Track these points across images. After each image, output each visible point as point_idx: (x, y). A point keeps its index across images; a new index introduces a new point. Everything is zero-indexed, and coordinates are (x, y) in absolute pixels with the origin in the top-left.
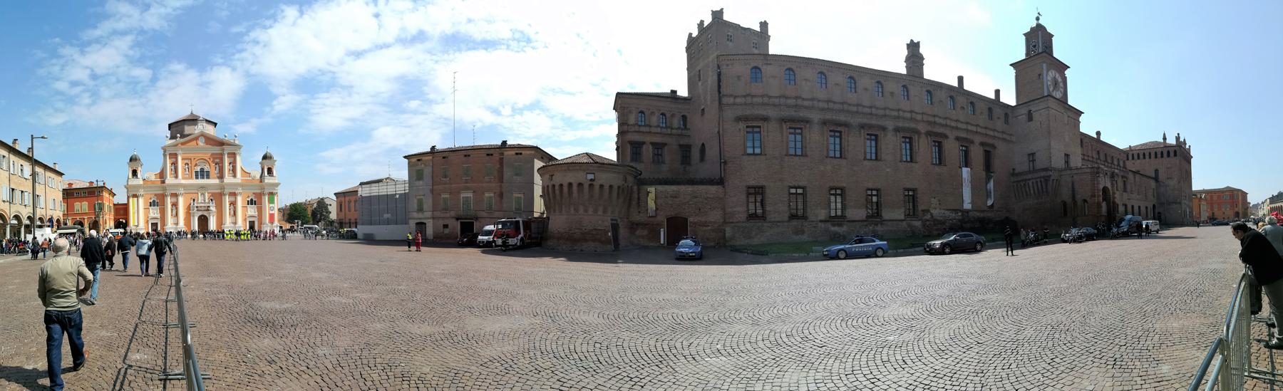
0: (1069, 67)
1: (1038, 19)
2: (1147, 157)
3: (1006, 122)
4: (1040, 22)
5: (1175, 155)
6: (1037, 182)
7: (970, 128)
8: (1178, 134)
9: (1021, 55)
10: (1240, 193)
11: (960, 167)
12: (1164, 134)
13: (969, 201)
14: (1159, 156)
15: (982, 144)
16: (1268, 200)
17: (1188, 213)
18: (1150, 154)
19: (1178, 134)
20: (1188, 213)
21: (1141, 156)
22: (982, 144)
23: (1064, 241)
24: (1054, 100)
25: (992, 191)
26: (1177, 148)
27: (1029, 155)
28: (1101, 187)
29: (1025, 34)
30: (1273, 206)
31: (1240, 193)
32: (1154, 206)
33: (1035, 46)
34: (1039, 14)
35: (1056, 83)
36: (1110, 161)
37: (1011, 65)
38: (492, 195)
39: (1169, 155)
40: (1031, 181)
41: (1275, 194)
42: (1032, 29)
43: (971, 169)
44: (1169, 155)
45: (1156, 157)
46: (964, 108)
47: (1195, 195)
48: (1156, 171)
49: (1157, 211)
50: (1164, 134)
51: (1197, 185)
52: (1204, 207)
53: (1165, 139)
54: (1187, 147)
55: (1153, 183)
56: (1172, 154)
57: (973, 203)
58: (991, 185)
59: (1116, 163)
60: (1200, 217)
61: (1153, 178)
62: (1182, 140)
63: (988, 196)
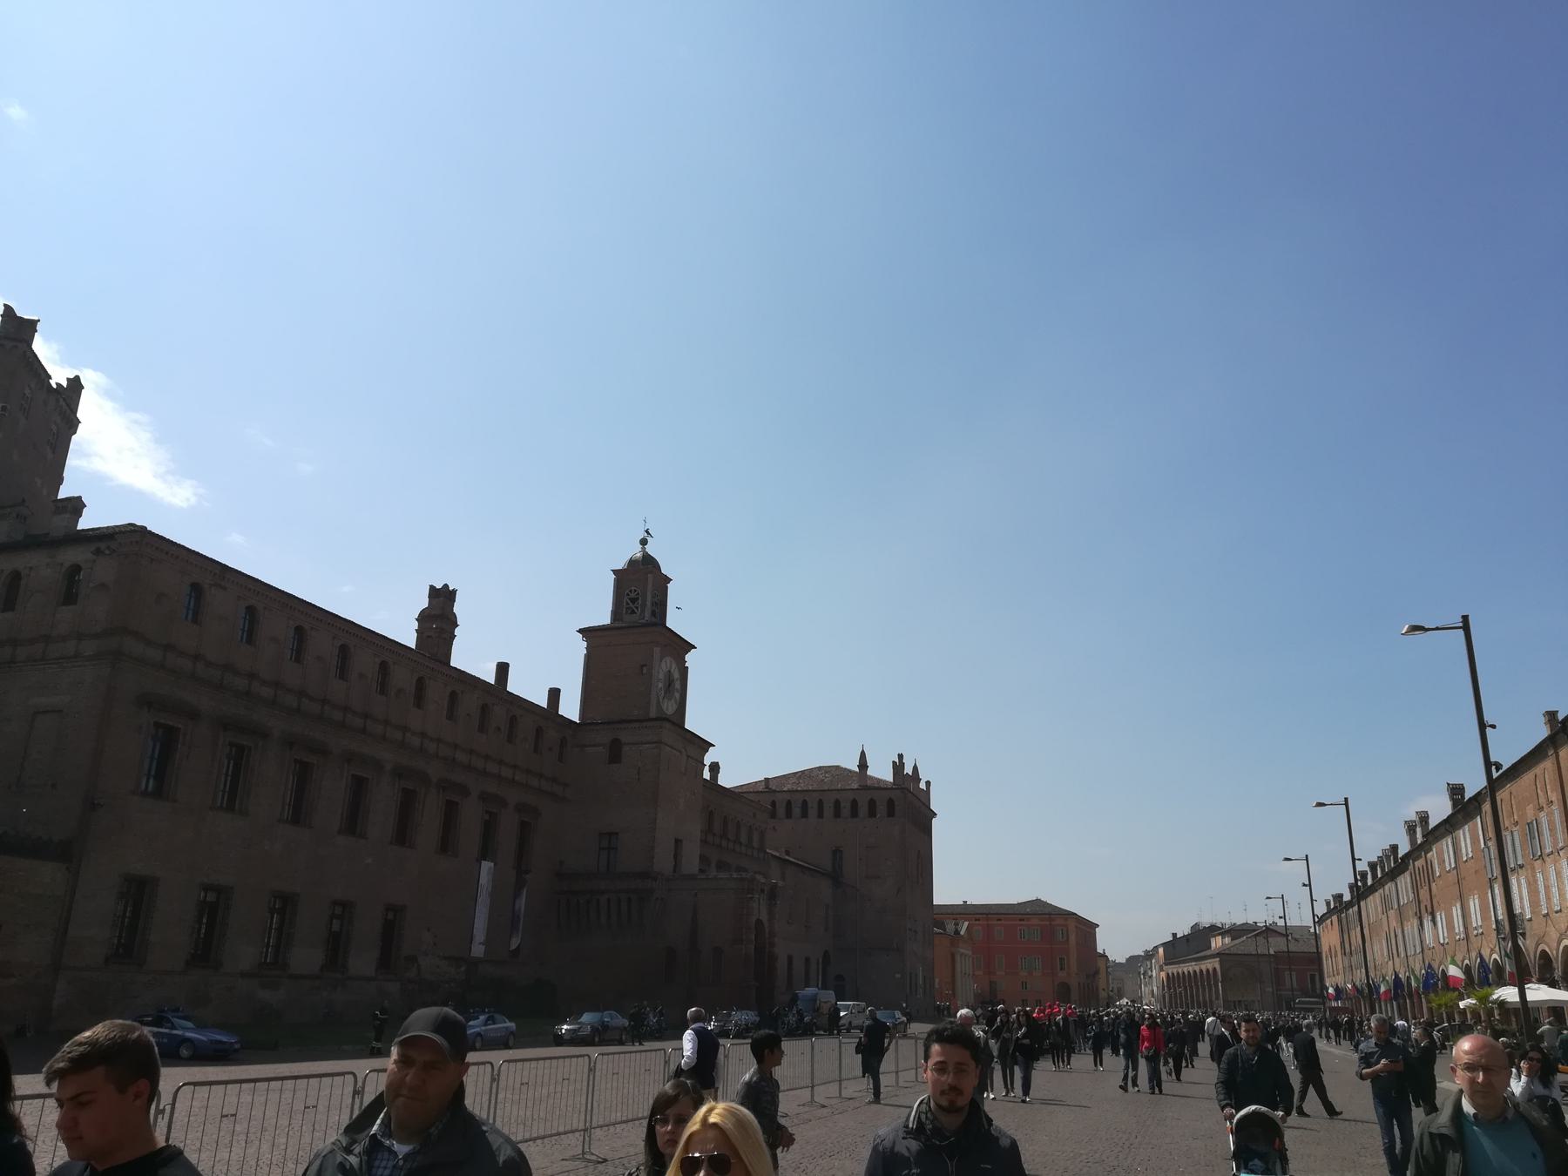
1: (644, 542)
2: (813, 812)
4: (650, 549)
5: (891, 812)
8: (901, 756)
9: (601, 614)
12: (863, 754)
16: (1161, 950)
17: (921, 981)
20: (921, 981)
21: (797, 811)
23: (559, 1041)
28: (754, 919)
30: (1173, 969)
32: (826, 955)
33: (634, 601)
34: (647, 532)
37: (580, 631)
39: (872, 812)
41: (1183, 930)
42: (632, 562)
44: (872, 812)
45: (837, 814)
46: (499, 729)
47: (941, 925)
48: (837, 853)
50: (863, 754)
51: (946, 891)
54: (922, 786)
56: (882, 809)
58: (522, 903)
59: (744, 839)
62: (908, 770)
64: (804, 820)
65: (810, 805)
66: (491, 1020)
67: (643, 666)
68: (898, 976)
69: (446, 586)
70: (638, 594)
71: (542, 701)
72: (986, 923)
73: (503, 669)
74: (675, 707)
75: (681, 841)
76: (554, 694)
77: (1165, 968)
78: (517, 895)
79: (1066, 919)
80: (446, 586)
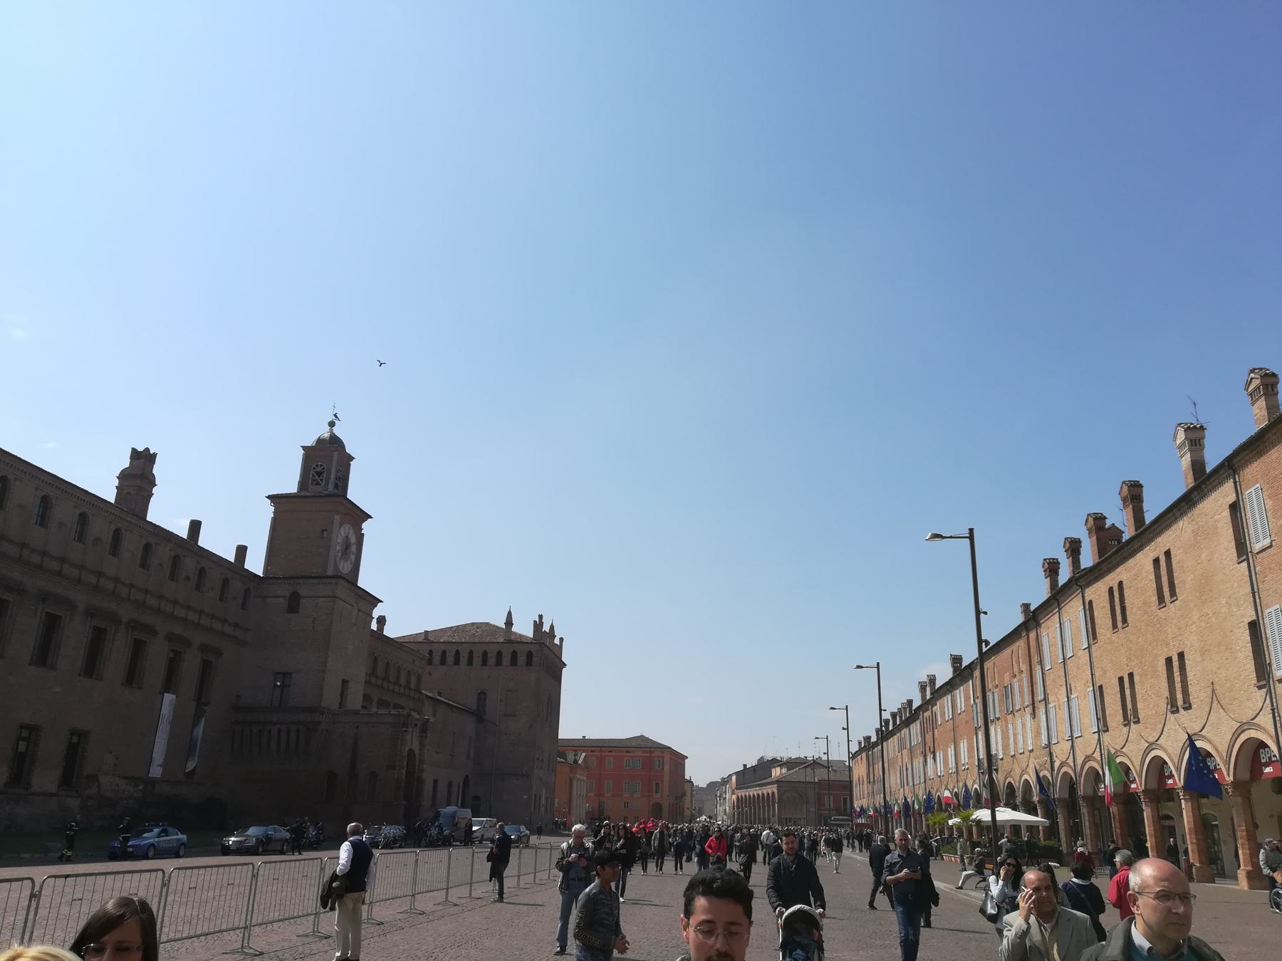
0: (370, 517)
1: (332, 424)
2: (464, 661)
4: (336, 430)
5: (529, 662)
6: (289, 731)
8: (541, 617)
10: (667, 756)
12: (510, 614)
13: (161, 761)
14: (492, 661)
16: (734, 778)
17: (543, 801)
18: (471, 653)
19: (541, 617)
20: (543, 801)
26: (533, 648)
28: (407, 749)
30: (742, 793)
31: (667, 756)
32: (466, 778)
33: (319, 474)
34: (335, 415)
35: (347, 547)
36: (392, 679)
37: (269, 497)
38: (768, 831)
39: (499, 662)
47: (563, 755)
48: (482, 695)
50: (510, 614)
51: (572, 725)
52: (581, 786)
53: (509, 623)
54: (557, 641)
55: (470, 725)
56: (522, 659)
57: (164, 765)
59: (403, 681)
60: (570, 813)
62: (546, 628)
63: (190, 752)
64: (456, 667)
65: (462, 655)
67: (323, 531)
68: (525, 797)
69: (147, 450)
70: (324, 468)
71: (231, 557)
72: (599, 754)
73: (195, 526)
74: (350, 567)
75: (348, 681)
76: (242, 551)
77: (736, 791)
78: (195, 723)
80: (147, 450)
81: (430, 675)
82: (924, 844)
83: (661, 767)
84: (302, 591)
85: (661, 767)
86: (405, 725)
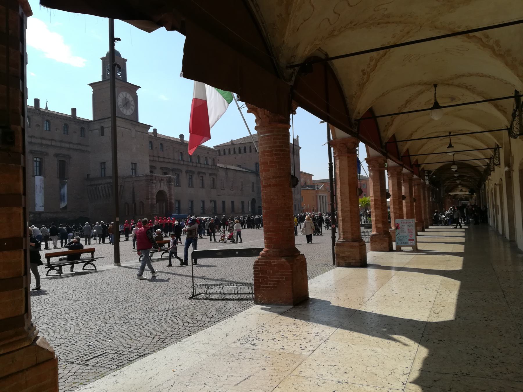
0: (140, 87)
2: (248, 151)
3: (83, 135)
7: (44, 142)
11: (34, 176)
15: (56, 155)
21: (242, 151)
22: (56, 155)
24: (122, 120)
25: (66, 195)
27: (101, 163)
29: (102, 59)
35: (126, 103)
37: (89, 85)
40: (101, 186)
43: (45, 177)
49: (257, 205)
57: (45, 205)
61: (252, 172)
63: (62, 198)
64: (245, 154)
65: (247, 148)
66: (202, 218)
71: (70, 113)
73: (74, 110)
76: (182, 136)
79: (366, 181)
81: (235, 158)
82: (30, 235)
83: (366, 187)
84: (104, 126)
85: (366, 187)
86: (151, 180)
